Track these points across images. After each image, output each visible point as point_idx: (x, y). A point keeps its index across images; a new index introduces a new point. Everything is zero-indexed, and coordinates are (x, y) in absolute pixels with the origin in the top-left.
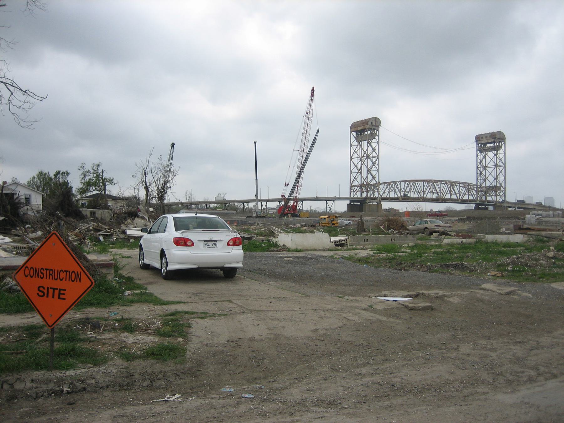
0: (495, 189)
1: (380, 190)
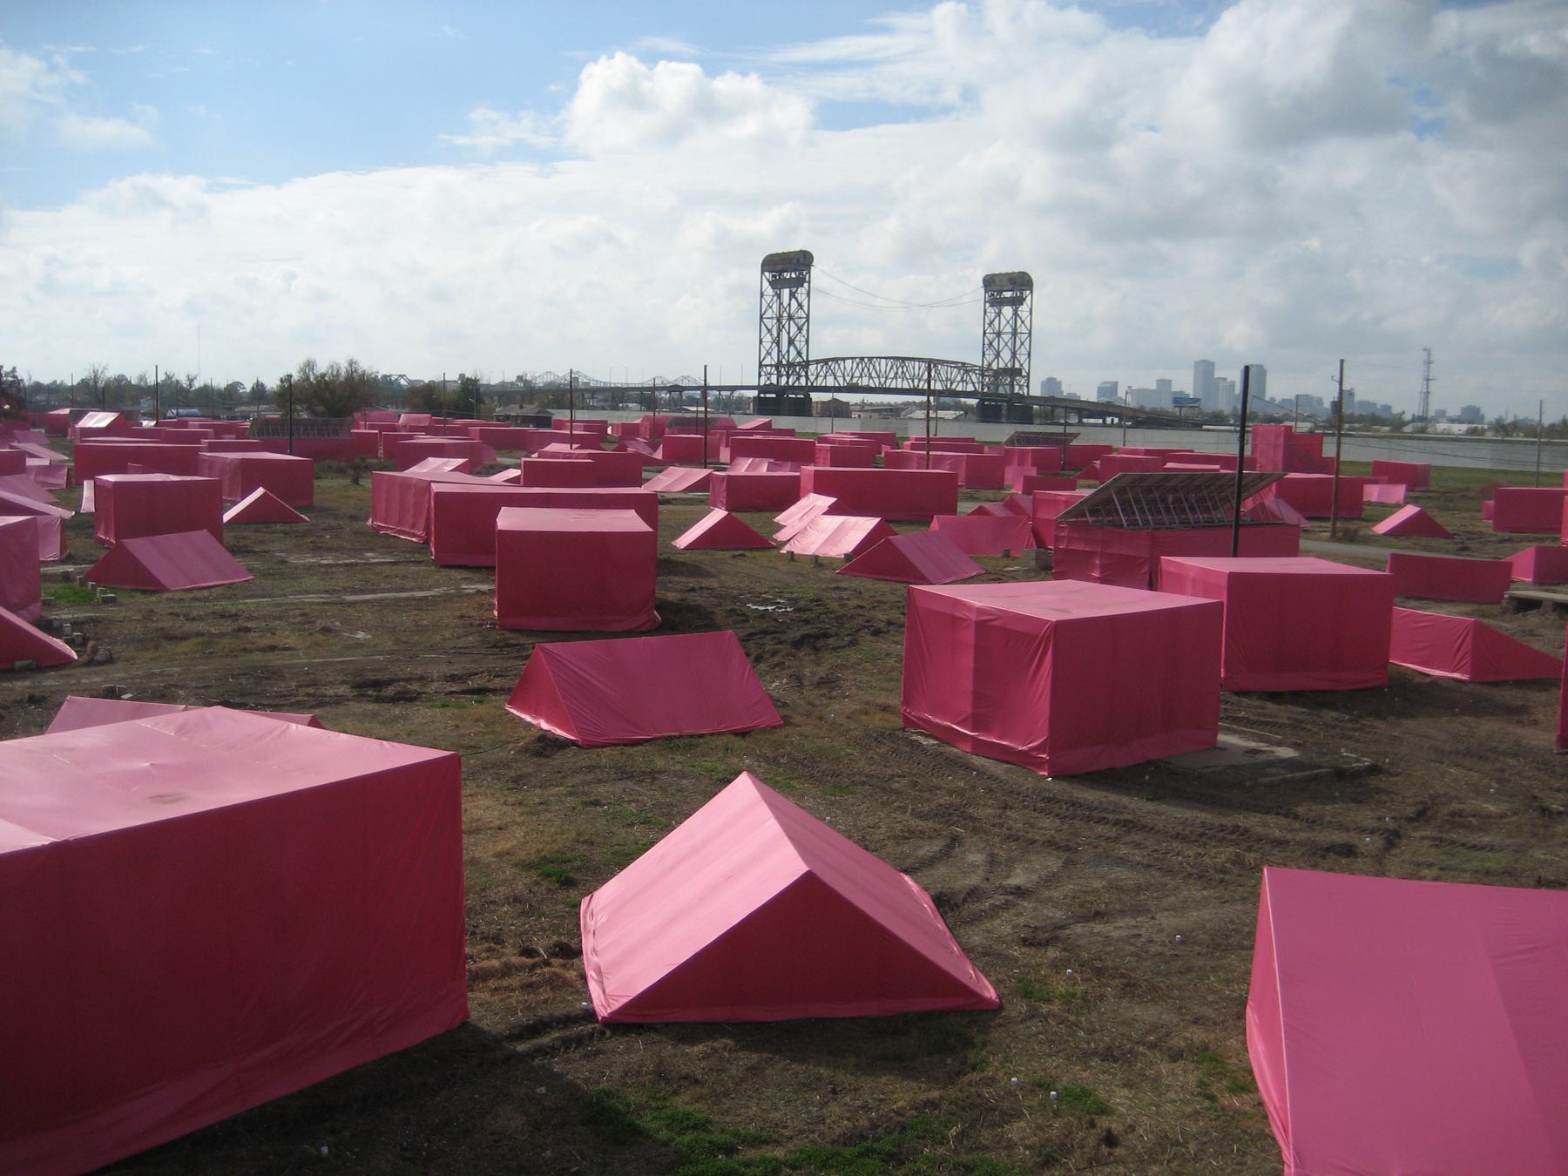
0: (1014, 372)
1: (809, 374)
